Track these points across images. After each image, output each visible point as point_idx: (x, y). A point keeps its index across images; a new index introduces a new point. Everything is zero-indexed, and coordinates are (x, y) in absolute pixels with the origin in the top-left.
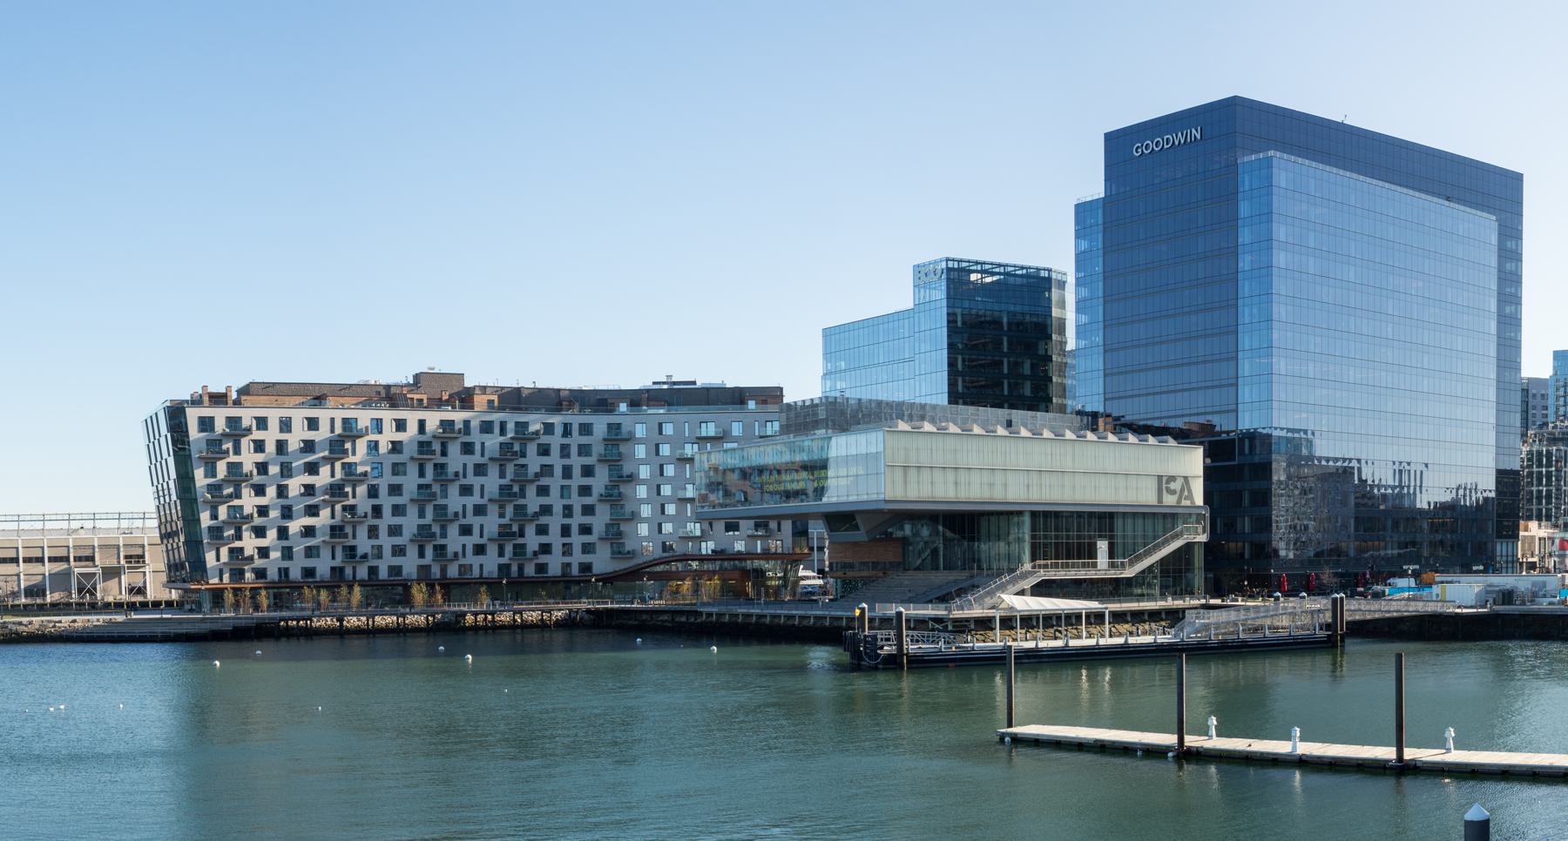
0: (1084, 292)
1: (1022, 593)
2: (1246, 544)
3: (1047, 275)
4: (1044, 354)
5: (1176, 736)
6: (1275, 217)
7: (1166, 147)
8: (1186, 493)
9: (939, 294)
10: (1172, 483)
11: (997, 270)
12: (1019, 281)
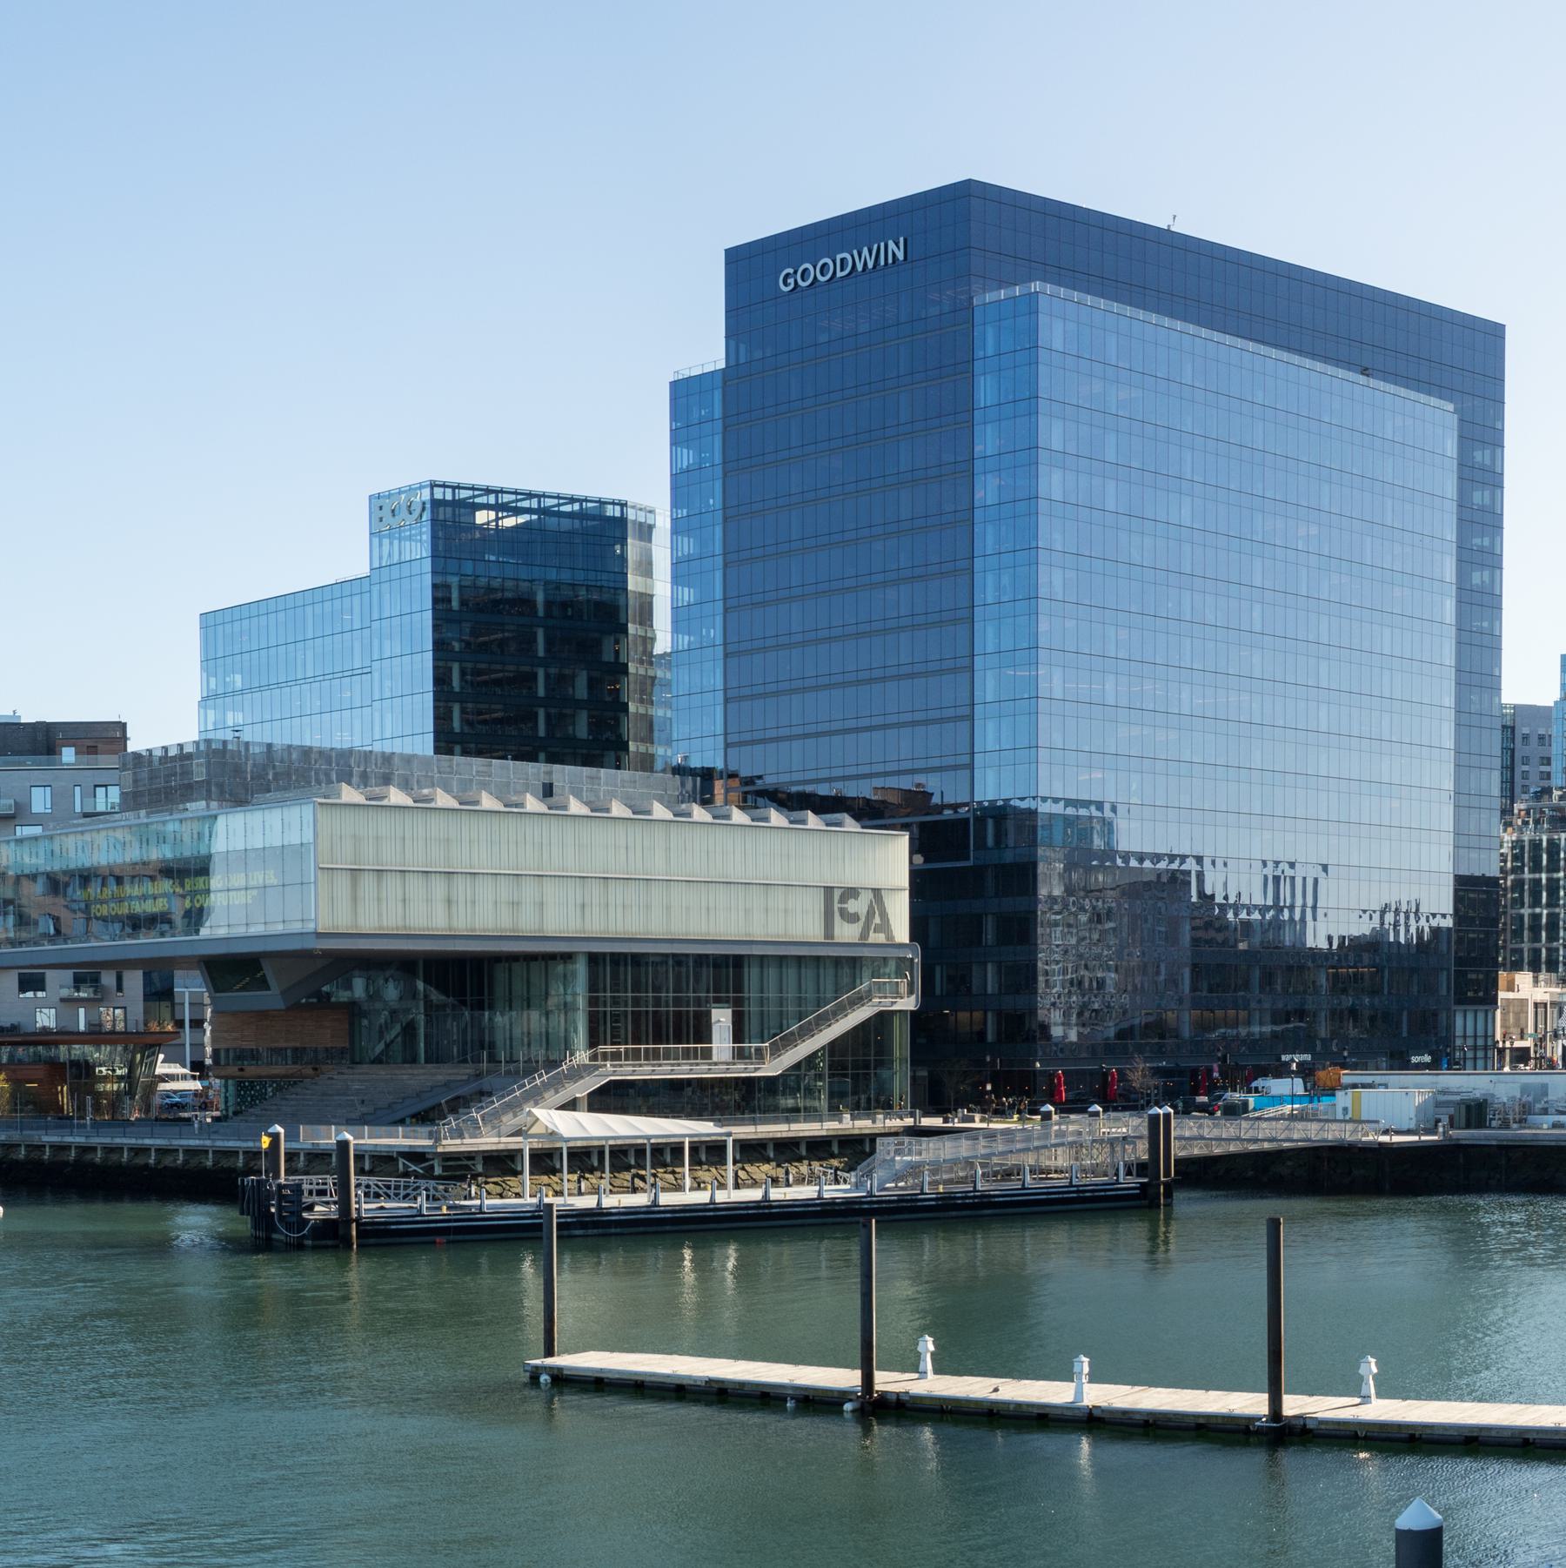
0: (688, 546)
1: (571, 1105)
2: (990, 1015)
3: (618, 514)
6: (1043, 405)
7: (839, 274)
8: (877, 920)
9: (418, 549)
10: (852, 901)
11: (526, 504)
12: (566, 524)
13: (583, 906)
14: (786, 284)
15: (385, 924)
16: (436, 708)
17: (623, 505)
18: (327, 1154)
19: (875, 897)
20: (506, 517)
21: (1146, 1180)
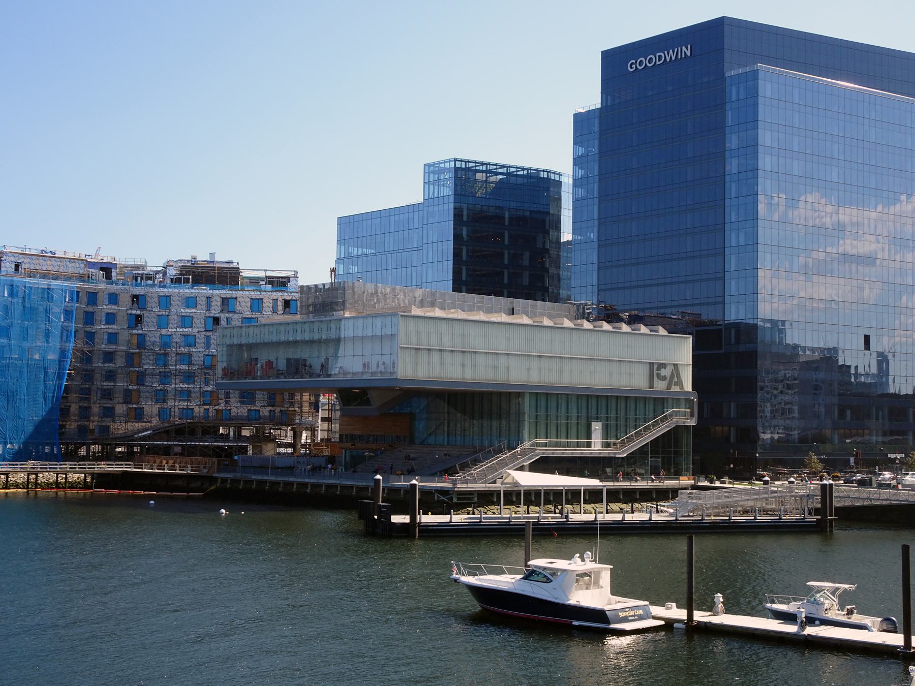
0: (581, 192)
1: (521, 469)
2: (732, 428)
3: (546, 176)
4: (541, 246)
5: (685, 611)
6: (760, 124)
7: (658, 63)
8: (676, 379)
9: (447, 191)
10: (663, 370)
11: (501, 170)
12: (520, 181)
13: (529, 369)
14: (631, 68)
15: (466, 377)
16: (454, 268)
17: (548, 172)
18: (399, 490)
19: (674, 368)
20: (491, 176)
21: (819, 517)
